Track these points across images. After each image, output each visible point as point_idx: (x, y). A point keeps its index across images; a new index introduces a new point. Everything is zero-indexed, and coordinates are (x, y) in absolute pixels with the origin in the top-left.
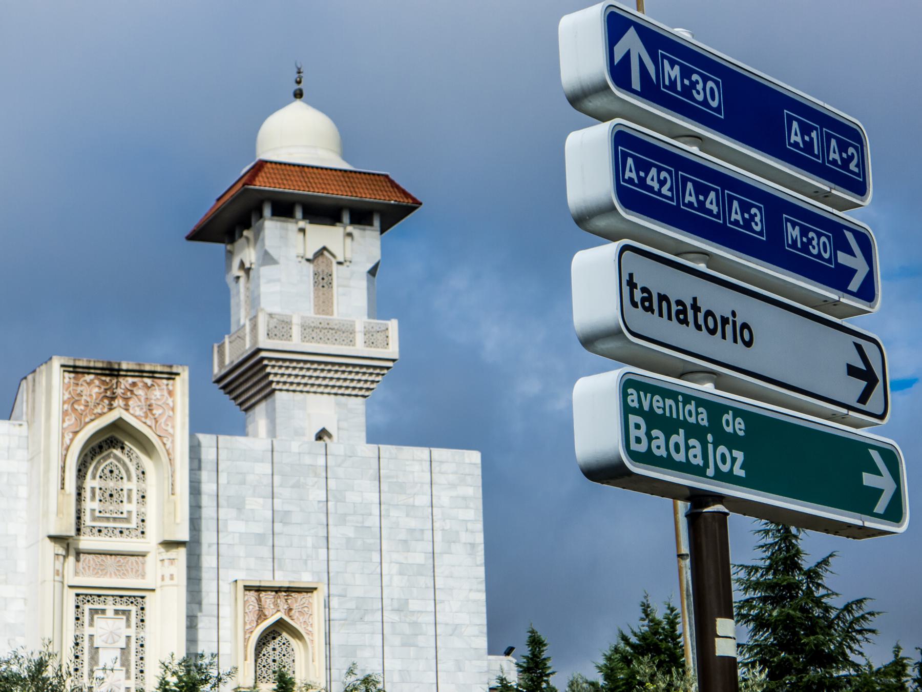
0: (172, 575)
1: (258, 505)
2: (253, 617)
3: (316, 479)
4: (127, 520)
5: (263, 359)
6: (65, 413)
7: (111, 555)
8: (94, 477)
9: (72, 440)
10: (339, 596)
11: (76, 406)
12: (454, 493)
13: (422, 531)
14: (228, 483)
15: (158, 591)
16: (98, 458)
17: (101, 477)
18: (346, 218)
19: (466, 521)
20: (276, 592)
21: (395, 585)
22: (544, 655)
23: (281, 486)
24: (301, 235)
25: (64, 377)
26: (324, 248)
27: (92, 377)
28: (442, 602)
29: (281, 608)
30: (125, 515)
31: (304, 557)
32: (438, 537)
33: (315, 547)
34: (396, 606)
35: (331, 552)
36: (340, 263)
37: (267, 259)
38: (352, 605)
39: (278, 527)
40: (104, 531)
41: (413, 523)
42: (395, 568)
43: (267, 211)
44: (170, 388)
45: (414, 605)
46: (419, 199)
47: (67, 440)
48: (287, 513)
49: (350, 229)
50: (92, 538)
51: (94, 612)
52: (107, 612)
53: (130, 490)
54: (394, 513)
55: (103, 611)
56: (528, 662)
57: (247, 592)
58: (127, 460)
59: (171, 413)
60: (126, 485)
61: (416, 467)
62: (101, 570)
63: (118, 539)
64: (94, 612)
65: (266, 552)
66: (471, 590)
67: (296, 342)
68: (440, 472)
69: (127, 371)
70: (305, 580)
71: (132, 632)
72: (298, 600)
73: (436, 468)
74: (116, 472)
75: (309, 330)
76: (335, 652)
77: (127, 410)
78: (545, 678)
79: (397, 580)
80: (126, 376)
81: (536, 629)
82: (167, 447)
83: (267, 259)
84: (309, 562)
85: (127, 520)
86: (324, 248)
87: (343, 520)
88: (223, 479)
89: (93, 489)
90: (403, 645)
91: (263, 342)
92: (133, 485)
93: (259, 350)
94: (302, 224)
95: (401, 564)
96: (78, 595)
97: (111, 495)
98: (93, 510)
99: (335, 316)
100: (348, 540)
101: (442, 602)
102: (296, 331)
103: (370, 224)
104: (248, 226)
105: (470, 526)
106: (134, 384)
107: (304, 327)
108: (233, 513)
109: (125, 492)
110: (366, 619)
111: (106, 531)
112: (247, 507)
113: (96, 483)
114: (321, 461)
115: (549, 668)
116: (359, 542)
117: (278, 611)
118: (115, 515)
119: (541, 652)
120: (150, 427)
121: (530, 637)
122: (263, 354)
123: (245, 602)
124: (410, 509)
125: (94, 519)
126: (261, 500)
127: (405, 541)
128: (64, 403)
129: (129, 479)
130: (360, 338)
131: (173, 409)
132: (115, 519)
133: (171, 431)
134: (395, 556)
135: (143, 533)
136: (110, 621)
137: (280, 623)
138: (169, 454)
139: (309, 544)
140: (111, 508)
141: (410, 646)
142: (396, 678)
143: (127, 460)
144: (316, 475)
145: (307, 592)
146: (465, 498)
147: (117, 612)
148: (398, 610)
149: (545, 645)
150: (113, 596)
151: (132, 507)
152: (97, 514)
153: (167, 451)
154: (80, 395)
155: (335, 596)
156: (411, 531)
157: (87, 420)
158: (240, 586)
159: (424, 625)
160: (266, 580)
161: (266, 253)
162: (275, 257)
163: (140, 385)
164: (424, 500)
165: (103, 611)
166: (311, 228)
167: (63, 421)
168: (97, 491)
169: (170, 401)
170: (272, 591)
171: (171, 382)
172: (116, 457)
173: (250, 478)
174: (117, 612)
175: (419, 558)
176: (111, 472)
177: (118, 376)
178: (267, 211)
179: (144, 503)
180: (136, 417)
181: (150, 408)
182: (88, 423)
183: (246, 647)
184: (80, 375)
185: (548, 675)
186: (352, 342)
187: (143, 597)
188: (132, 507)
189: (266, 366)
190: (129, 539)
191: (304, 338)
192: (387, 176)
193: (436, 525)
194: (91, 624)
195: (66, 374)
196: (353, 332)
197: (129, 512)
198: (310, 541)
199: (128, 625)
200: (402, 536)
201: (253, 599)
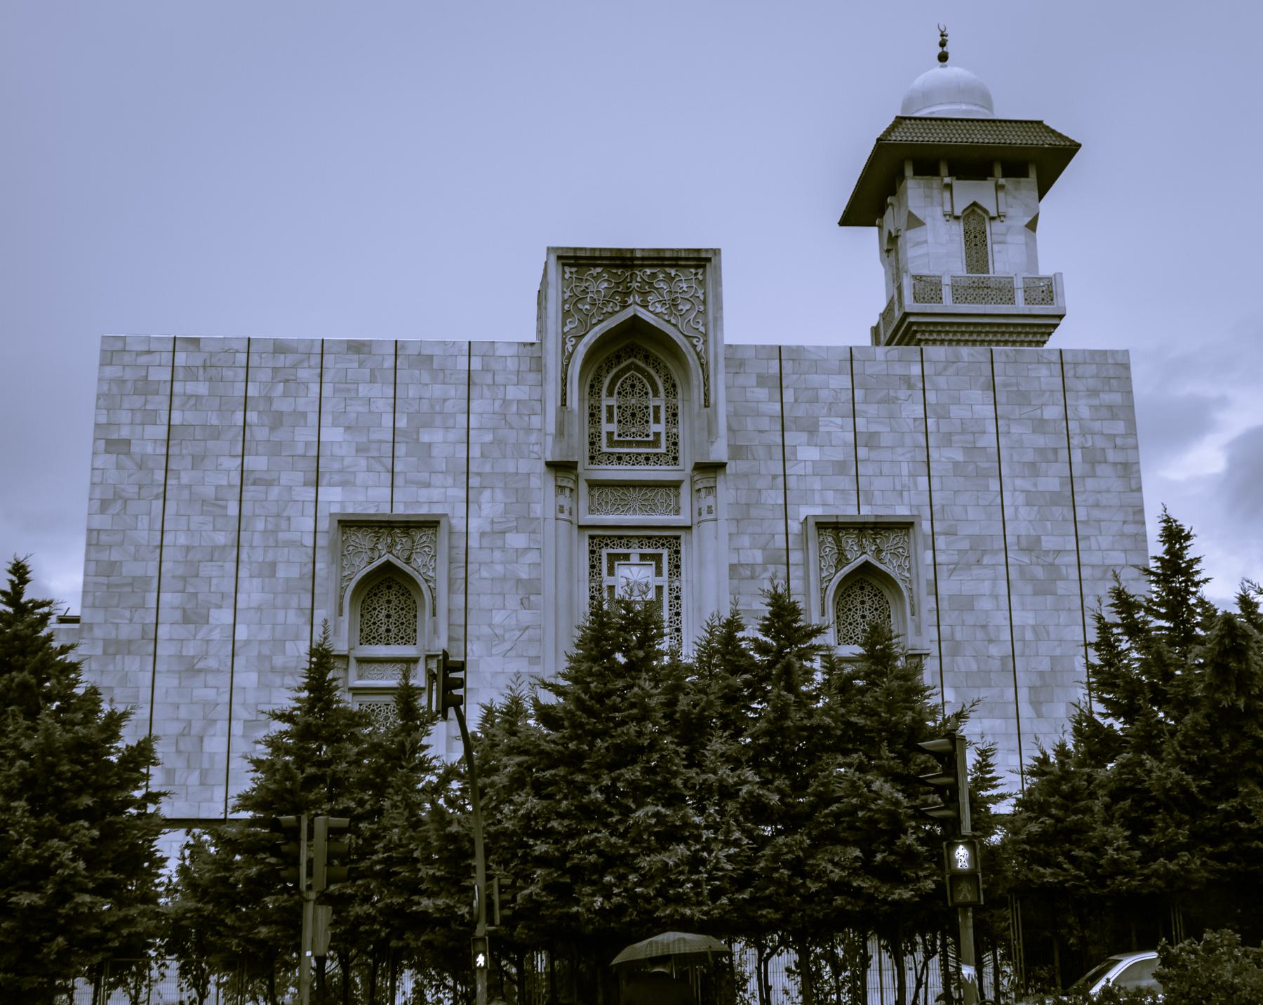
0: (710, 507)
1: (837, 429)
2: (832, 560)
3: (910, 392)
4: (655, 443)
5: (911, 324)
6: (566, 314)
7: (634, 487)
8: (610, 394)
9: (575, 346)
10: (946, 534)
11: (580, 306)
12: (1096, 402)
13: (1055, 450)
14: (796, 401)
15: (694, 530)
16: (614, 371)
17: (619, 393)
18: (998, 170)
19: (1115, 436)
20: (860, 530)
21: (1021, 522)
22: (1190, 554)
23: (865, 402)
24: (947, 194)
25: (564, 272)
26: (975, 204)
27: (599, 270)
28: (1088, 538)
29: (867, 549)
30: (651, 438)
31: (898, 487)
32: (1077, 456)
33: (913, 475)
34: (1024, 544)
35: (934, 481)
36: (993, 219)
37: (914, 222)
38: (965, 545)
39: (862, 452)
40: (653, 459)
41: (1040, 441)
42: (1021, 498)
43: (909, 171)
44: (700, 277)
45: (1048, 543)
46: (1078, 141)
47: (569, 347)
48: (873, 435)
49: (1002, 181)
50: (610, 467)
51: (617, 557)
52: (632, 557)
53: (657, 408)
54: (1016, 429)
55: (626, 557)
56: (1163, 567)
57: (822, 531)
58: (653, 372)
59: (702, 308)
60: (652, 402)
61: (1044, 372)
62: (624, 506)
63: (643, 467)
64: (613, 558)
65: (847, 483)
66: (1125, 522)
67: (948, 304)
68: (1075, 377)
69: (643, 259)
70: (902, 511)
71: (664, 581)
72: (890, 542)
73: (1069, 372)
74: (639, 386)
75: (960, 291)
76: (944, 605)
77: (645, 307)
78: (1193, 589)
79: (1023, 511)
80: (643, 266)
81: (1174, 516)
82: (698, 349)
83: (914, 222)
84: (905, 494)
85: (655, 443)
86: (975, 204)
87: (947, 440)
88: (789, 396)
89: (610, 408)
90: (1035, 594)
91: (910, 305)
92: (661, 401)
93: (906, 315)
94: (947, 180)
95: (1027, 492)
96: (592, 537)
97: (633, 415)
98: (610, 434)
99: (991, 274)
100: (956, 464)
101: (1088, 538)
102: (947, 293)
103: (1027, 176)
104: (893, 192)
105: (1119, 441)
106: (654, 275)
107: (955, 288)
108: (804, 437)
109: (651, 410)
110: (985, 562)
111: (628, 458)
112: (821, 429)
113: (613, 401)
114: (916, 370)
115: (1198, 572)
116: (971, 467)
117: (863, 553)
118: (638, 439)
119: (1183, 548)
120: (674, 325)
121: (1165, 529)
122: (912, 319)
123: (821, 543)
124: (1040, 425)
125: (611, 443)
126: (839, 421)
127: (1033, 464)
128: (565, 302)
129: (656, 394)
130: (1020, 296)
131: (704, 302)
132: (639, 444)
133: (702, 329)
134: (1019, 483)
135: (675, 459)
136: (635, 569)
137: (866, 566)
138: (699, 358)
139: (905, 472)
140: (633, 430)
141: (1044, 593)
142: (1029, 635)
143: (653, 372)
144: (910, 387)
145: (901, 529)
146: (1110, 407)
147: (643, 557)
148: (1029, 550)
149: (1188, 537)
150: (638, 537)
151: (661, 428)
152: (616, 438)
153: (698, 354)
154: (585, 291)
155: (941, 534)
156: (1040, 451)
157: (594, 321)
158: (811, 523)
159: (1064, 569)
160: (848, 511)
161: (911, 215)
162: (921, 218)
163: (661, 276)
164: (1053, 412)
165: (626, 557)
166: (958, 185)
167: (564, 325)
168: (616, 410)
169: (700, 294)
170: (855, 529)
171: (700, 271)
172: (638, 369)
173: (823, 394)
174: (643, 557)
175: (1051, 482)
176: (633, 386)
177: (633, 266)
178: (909, 171)
179: (675, 423)
180: (656, 314)
181: (674, 304)
182: (595, 324)
183: (823, 599)
184: (585, 269)
185: (1197, 584)
186: (1011, 300)
187: (678, 538)
188: (661, 428)
189: (916, 332)
190: (657, 467)
191: (956, 300)
192: (1040, 123)
193: (1074, 442)
194: (611, 572)
195: (567, 269)
196: (1012, 290)
197: (657, 435)
198: (905, 469)
199: (659, 573)
200: (1029, 456)
201: (830, 539)
